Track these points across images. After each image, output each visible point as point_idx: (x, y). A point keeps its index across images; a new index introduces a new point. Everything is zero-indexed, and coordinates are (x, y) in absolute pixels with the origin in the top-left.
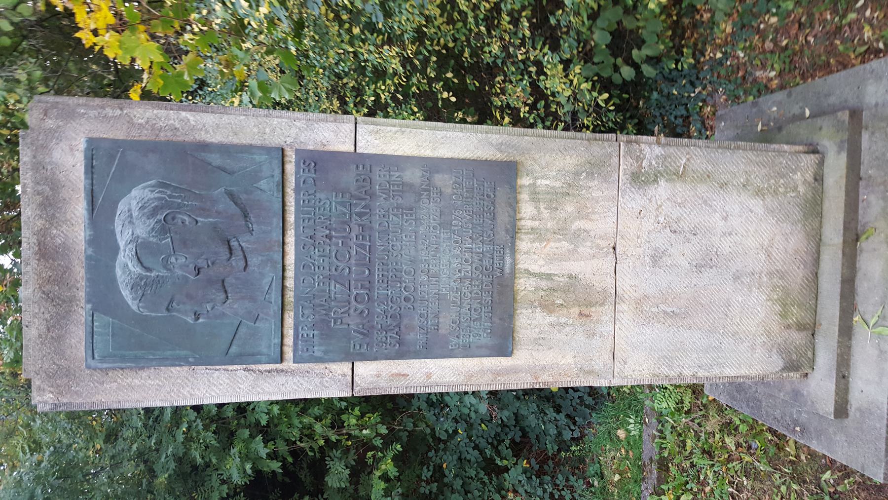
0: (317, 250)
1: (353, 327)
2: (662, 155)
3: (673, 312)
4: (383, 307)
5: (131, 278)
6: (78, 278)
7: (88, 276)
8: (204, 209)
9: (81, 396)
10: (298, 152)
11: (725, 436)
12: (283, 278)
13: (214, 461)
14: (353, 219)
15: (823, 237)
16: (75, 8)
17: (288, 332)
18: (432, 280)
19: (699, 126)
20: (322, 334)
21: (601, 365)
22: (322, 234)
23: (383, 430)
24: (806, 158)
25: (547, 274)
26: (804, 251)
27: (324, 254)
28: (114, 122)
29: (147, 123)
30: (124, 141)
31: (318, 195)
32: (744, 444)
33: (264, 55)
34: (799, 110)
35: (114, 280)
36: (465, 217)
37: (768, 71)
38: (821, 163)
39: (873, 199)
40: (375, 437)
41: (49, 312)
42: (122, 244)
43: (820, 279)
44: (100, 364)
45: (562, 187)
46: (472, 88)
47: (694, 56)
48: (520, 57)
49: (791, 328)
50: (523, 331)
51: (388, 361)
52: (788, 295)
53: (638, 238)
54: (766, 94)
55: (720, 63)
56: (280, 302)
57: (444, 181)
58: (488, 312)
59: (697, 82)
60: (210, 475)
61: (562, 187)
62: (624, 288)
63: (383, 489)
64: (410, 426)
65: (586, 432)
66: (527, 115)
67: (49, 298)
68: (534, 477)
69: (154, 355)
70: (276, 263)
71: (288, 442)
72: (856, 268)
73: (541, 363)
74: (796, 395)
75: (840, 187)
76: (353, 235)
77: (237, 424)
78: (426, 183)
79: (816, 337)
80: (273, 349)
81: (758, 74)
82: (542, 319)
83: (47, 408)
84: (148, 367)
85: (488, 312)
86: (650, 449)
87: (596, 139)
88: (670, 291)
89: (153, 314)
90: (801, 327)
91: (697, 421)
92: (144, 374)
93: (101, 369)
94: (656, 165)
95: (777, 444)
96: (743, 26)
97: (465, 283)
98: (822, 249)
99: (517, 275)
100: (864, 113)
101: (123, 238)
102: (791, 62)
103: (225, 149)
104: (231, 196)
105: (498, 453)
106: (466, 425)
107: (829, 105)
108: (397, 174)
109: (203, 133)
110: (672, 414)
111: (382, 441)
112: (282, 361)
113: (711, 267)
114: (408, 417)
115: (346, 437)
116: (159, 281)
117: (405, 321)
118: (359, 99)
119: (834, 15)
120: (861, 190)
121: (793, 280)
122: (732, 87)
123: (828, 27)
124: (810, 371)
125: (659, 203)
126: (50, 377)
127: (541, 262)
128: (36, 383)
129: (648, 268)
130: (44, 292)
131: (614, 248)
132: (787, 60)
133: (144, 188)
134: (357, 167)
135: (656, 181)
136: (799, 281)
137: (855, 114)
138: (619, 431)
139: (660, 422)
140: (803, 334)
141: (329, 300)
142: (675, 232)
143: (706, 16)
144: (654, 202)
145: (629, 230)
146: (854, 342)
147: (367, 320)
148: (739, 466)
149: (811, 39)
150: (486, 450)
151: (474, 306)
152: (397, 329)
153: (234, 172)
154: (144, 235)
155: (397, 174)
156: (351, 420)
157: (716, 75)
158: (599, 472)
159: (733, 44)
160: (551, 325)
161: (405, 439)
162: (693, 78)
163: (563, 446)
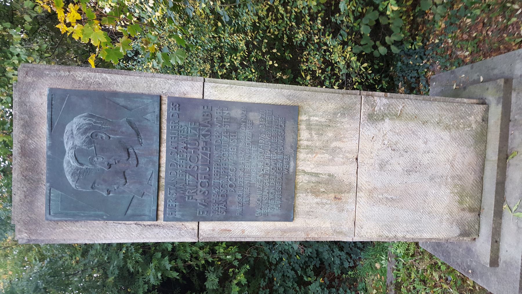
0: (179, 155)
1: (199, 201)
2: (387, 104)
3: (392, 198)
4: (217, 190)
5: (72, 169)
6: (43, 168)
7: (48, 167)
8: (114, 131)
9: (43, 236)
10: (169, 98)
11: (433, 271)
12: (159, 171)
13: (140, 270)
14: (200, 138)
15: (487, 156)
16: (57, 10)
17: (161, 203)
18: (246, 175)
19: (424, 83)
20: (180, 205)
21: (347, 228)
22: (182, 146)
23: (239, 256)
24: (477, 107)
25: (316, 173)
26: (475, 164)
27: (183, 158)
28: (65, 79)
29: (84, 80)
30: (70, 90)
31: (180, 123)
32: (444, 278)
33: (168, 38)
34: (477, 77)
35: (62, 169)
36: (267, 139)
37: (465, 51)
38: (487, 111)
39: (517, 133)
40: (234, 260)
41: (26, 187)
42: (67, 149)
43: (484, 181)
44: (53, 218)
45: (326, 122)
46: (288, 58)
47: (422, 42)
48: (316, 41)
49: (465, 210)
50: (300, 207)
51: (219, 222)
52: (464, 190)
53: (371, 153)
54: (462, 66)
55: (438, 46)
56: (157, 185)
57: (255, 117)
58: (280, 195)
59: (424, 57)
60: (139, 279)
61: (326, 122)
62: (362, 183)
63: (238, 291)
64: (255, 255)
65: (358, 263)
66: (320, 75)
67: (26, 178)
68: (325, 289)
69: (84, 214)
70: (155, 162)
71: (185, 262)
72: (506, 175)
73: (311, 226)
74: (469, 250)
75: (497, 126)
76: (200, 147)
77: (155, 249)
78: (244, 118)
79: (481, 217)
80: (152, 213)
81: (459, 53)
82: (312, 200)
83: (24, 241)
84: (81, 221)
85: (280, 195)
86: (391, 276)
87: (347, 94)
88: (390, 185)
89: (84, 190)
90: (471, 210)
91: (417, 261)
92: (78, 224)
93: (54, 221)
94: (383, 110)
95: (462, 279)
96: (451, 24)
97: (266, 177)
98: (486, 163)
99: (298, 173)
100: (514, 80)
101: (68, 146)
102: (478, 46)
103: (127, 96)
104: (130, 123)
105: (306, 273)
106: (287, 256)
107: (494, 75)
108: (227, 112)
109: (115, 86)
110: (403, 257)
111: (238, 263)
112: (157, 219)
113: (416, 172)
114: (254, 249)
115: (217, 259)
116: (87, 171)
117: (230, 198)
118: (221, 64)
119: (503, 19)
120: (511, 128)
121: (467, 181)
122: (443, 60)
123: (499, 26)
124: (476, 237)
125: (385, 133)
126: (26, 224)
127: (312, 166)
128: (18, 227)
129: (377, 172)
130: (23, 176)
131: (357, 159)
132: (476, 46)
133: (81, 117)
134: (204, 107)
135: (383, 119)
136: (471, 182)
137: (508, 81)
138: (376, 264)
139: (397, 261)
140: (473, 214)
141: (185, 185)
142: (394, 150)
143: (431, 17)
144: (381, 132)
145: (366, 148)
146: (503, 221)
147: (207, 197)
148: (440, 290)
149: (490, 33)
150: (298, 272)
151: (271, 191)
152: (225, 203)
153: (132, 110)
154: (79, 145)
155: (227, 112)
156: (220, 250)
157: (435, 53)
158: (364, 288)
159: (445, 35)
160: (317, 203)
161: (252, 262)
162: (422, 54)
163: (344, 271)
